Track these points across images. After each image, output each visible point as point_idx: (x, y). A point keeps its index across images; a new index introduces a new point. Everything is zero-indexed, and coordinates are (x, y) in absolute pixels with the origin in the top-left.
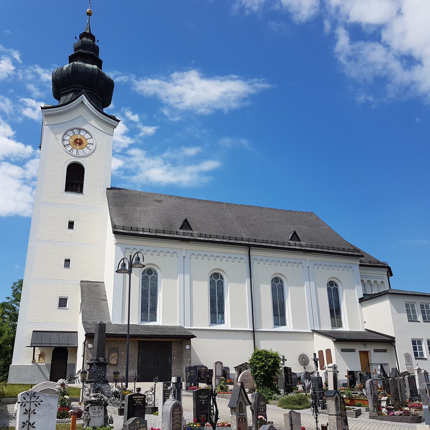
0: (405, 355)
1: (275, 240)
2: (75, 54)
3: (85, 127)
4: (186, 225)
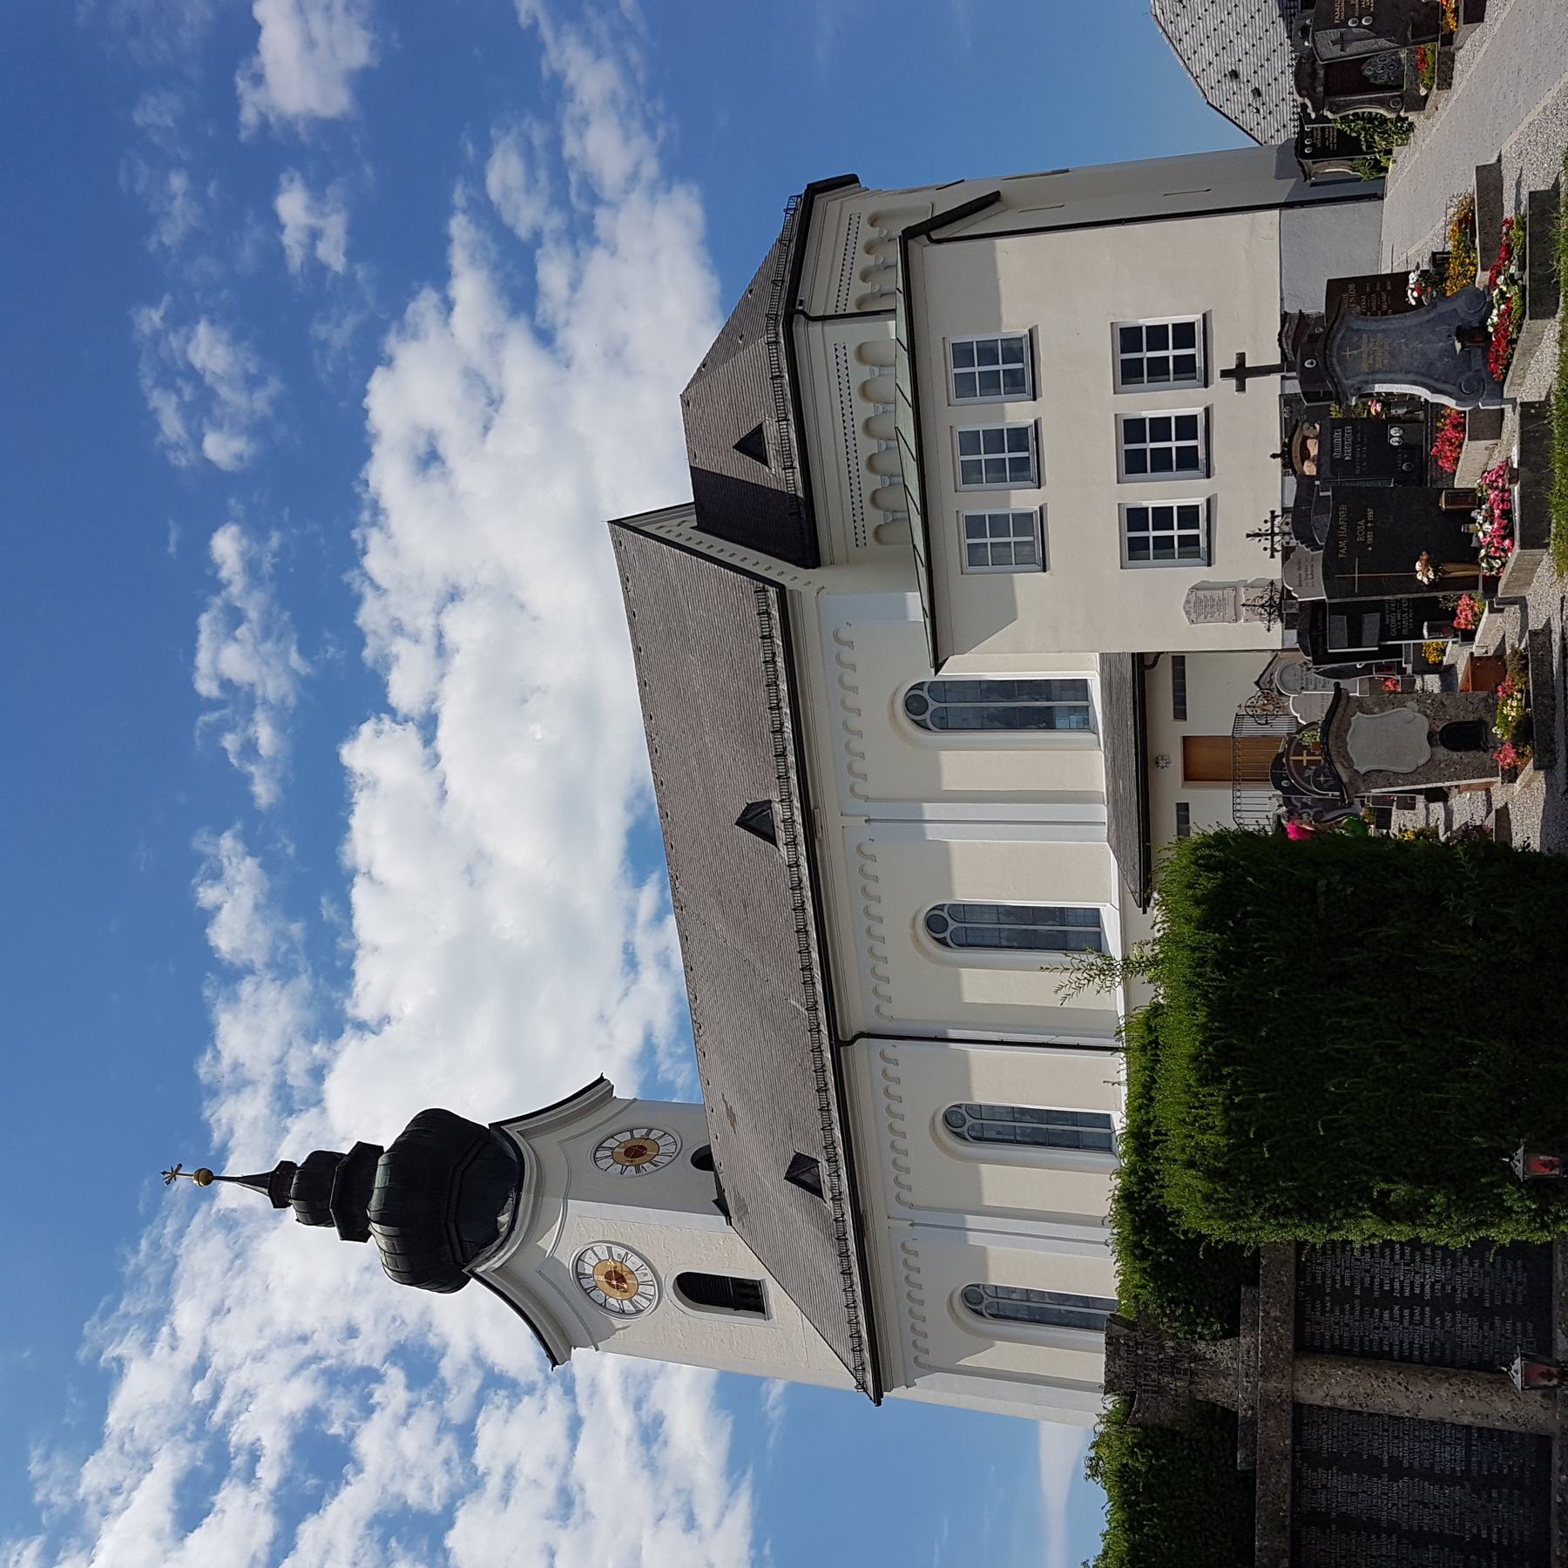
0: (1193, 616)
1: (789, 899)
2: (339, 1227)
3: (568, 1263)
4: (756, 820)
